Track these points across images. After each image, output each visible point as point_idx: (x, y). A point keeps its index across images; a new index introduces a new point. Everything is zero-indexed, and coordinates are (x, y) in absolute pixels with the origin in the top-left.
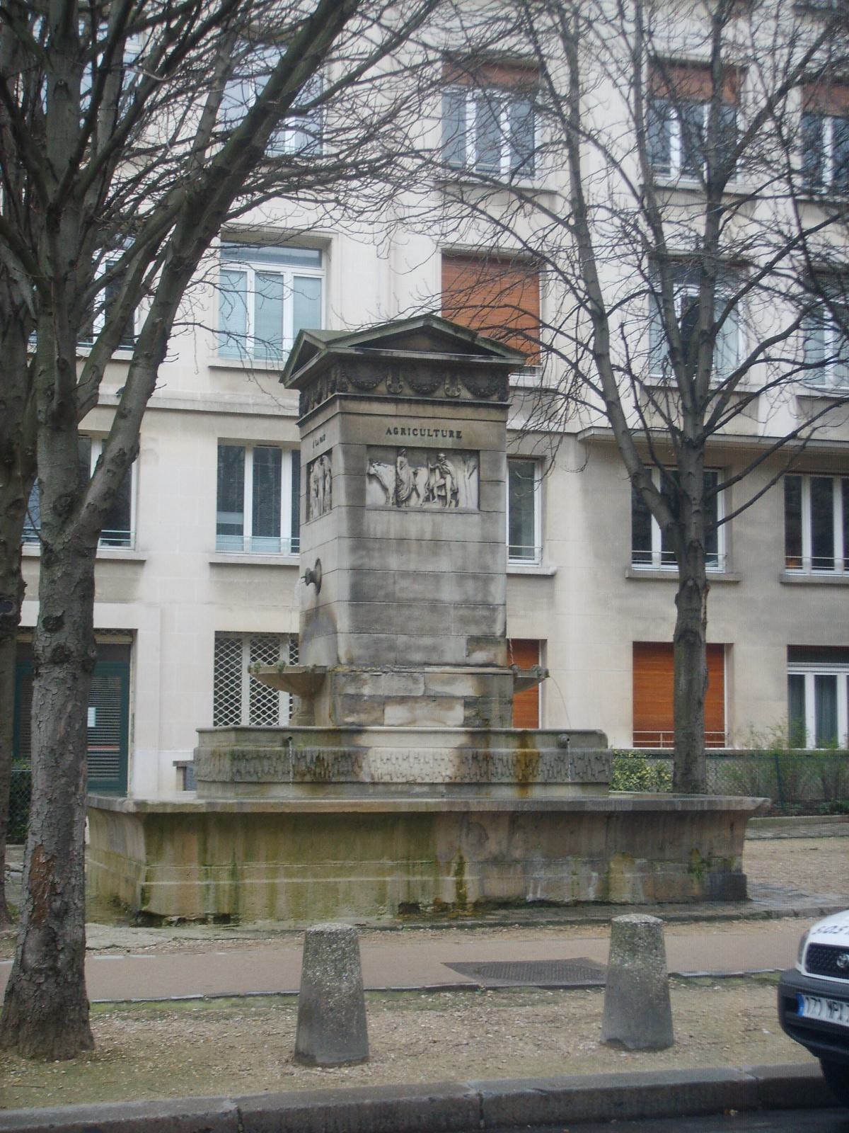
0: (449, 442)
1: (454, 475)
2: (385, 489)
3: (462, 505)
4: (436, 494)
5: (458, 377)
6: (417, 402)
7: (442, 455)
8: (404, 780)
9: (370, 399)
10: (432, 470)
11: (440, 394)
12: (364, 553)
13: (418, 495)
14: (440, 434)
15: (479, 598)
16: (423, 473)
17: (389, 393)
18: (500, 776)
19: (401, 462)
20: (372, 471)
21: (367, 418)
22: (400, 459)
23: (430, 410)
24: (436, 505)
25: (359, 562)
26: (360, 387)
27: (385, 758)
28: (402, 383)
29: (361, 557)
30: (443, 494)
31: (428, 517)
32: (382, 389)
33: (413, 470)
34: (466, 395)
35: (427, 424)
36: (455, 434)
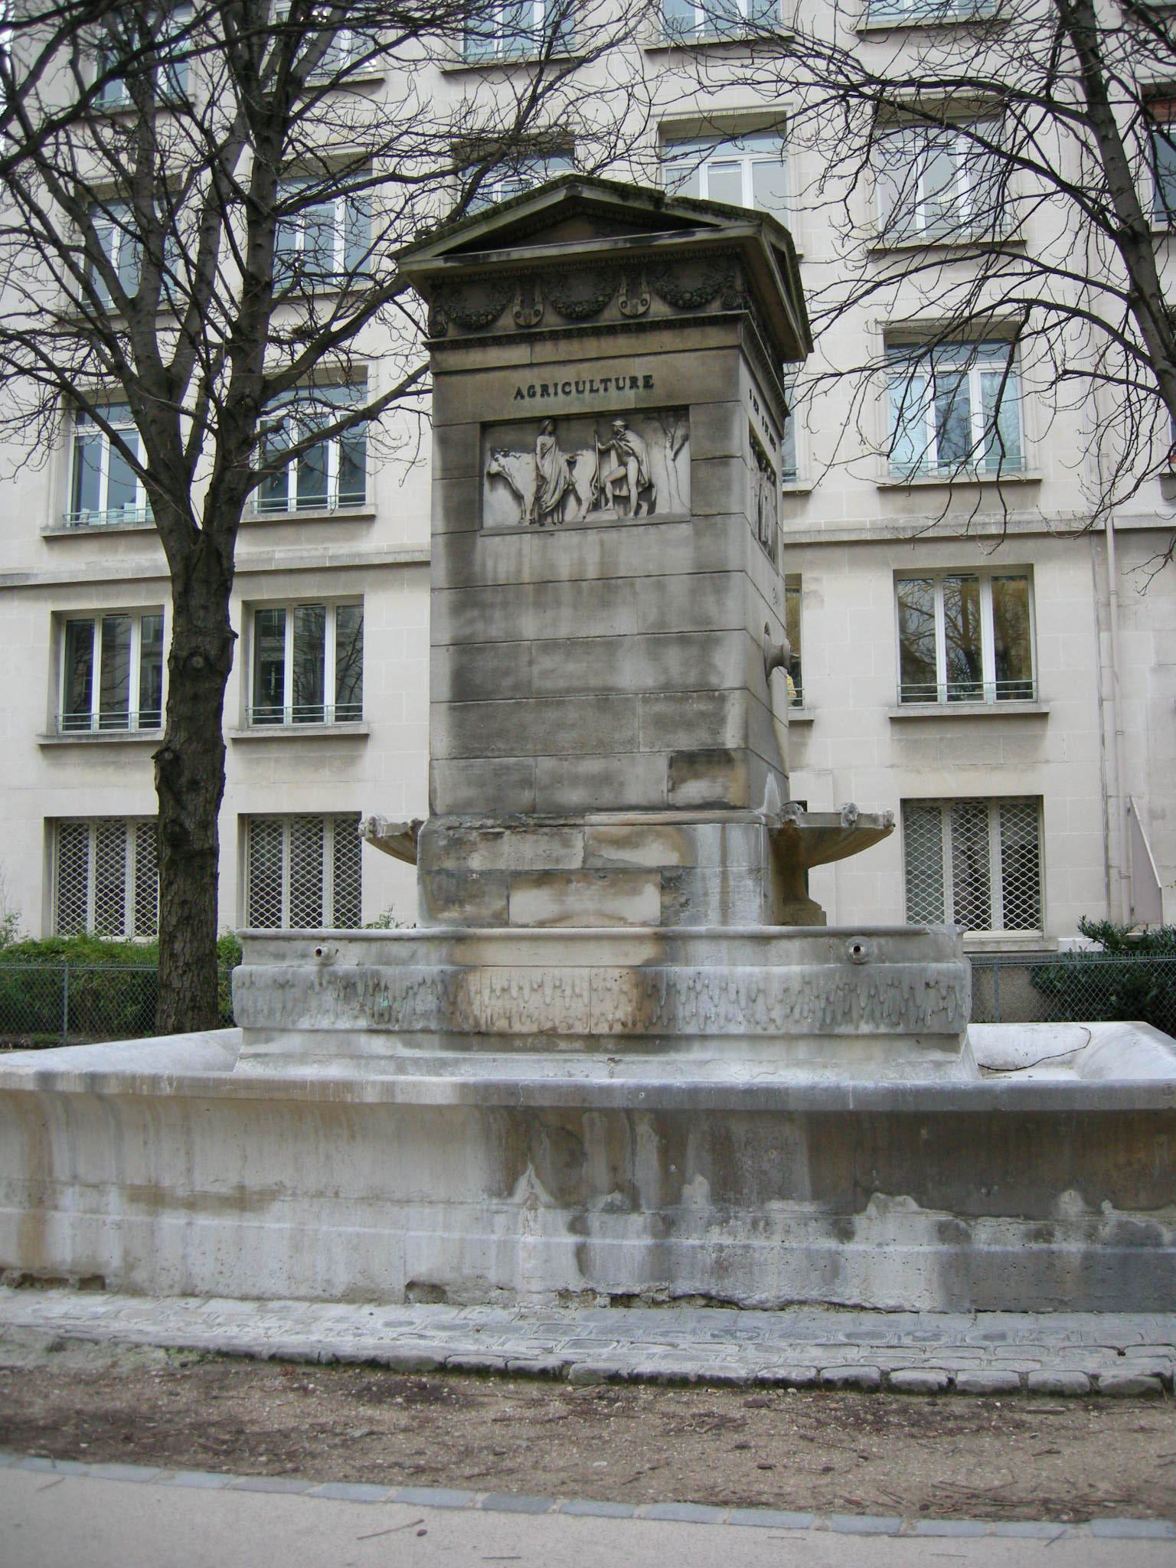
0: (629, 398)
1: (643, 456)
2: (518, 497)
3: (662, 508)
4: (610, 496)
5: (643, 279)
6: (568, 335)
7: (619, 423)
8: (534, 1028)
9: (483, 343)
10: (603, 454)
11: (611, 315)
12: (476, 613)
13: (579, 501)
14: (612, 386)
15: (692, 678)
16: (587, 461)
17: (519, 326)
18: (722, 1021)
19: (543, 445)
20: (494, 468)
21: (479, 377)
22: (540, 440)
23: (592, 347)
24: (609, 514)
25: (467, 631)
26: (465, 325)
27: (498, 987)
28: (540, 307)
29: (471, 622)
30: (624, 493)
31: (592, 536)
32: (507, 323)
33: (567, 457)
34: (659, 309)
35: (586, 371)
36: (641, 383)
